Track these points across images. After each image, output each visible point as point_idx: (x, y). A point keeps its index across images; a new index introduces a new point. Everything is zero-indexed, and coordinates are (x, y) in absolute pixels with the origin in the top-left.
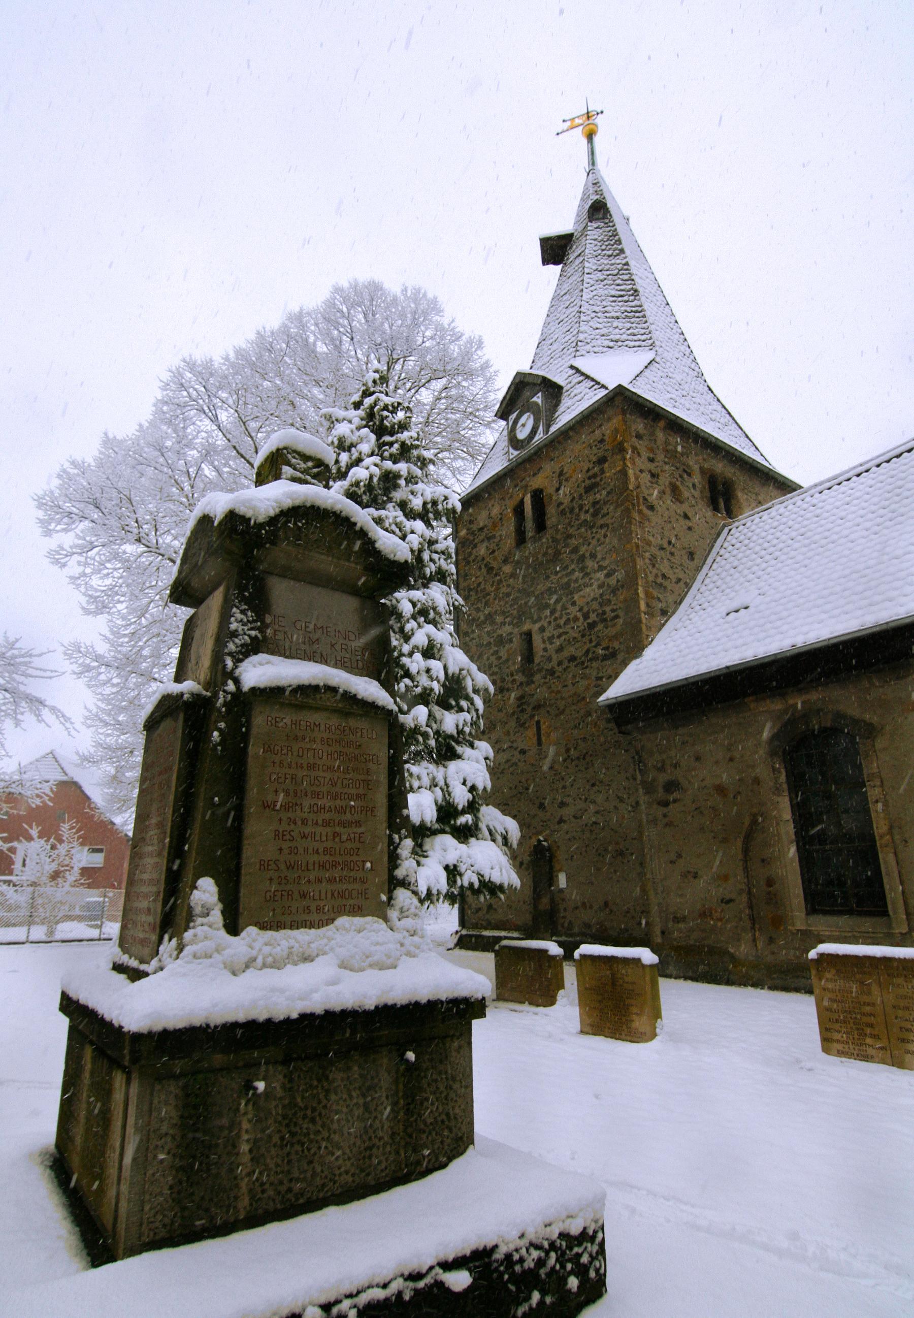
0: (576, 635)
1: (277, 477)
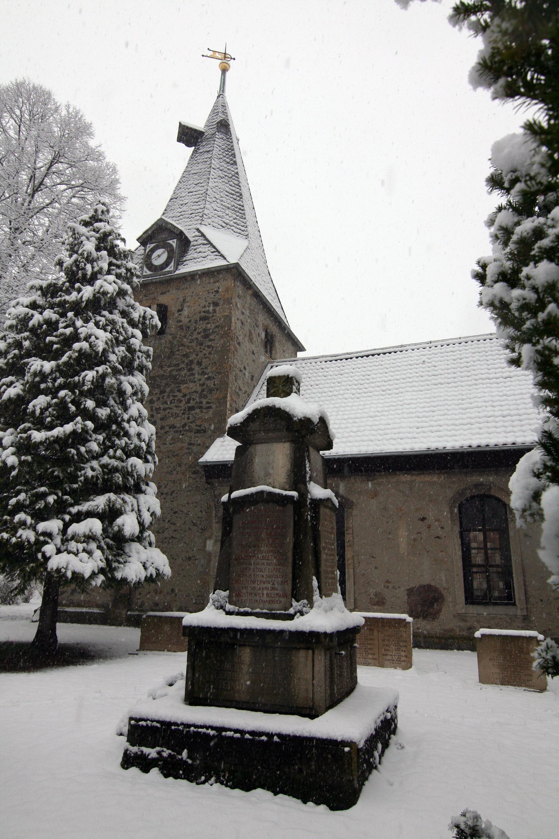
0: (177, 412)
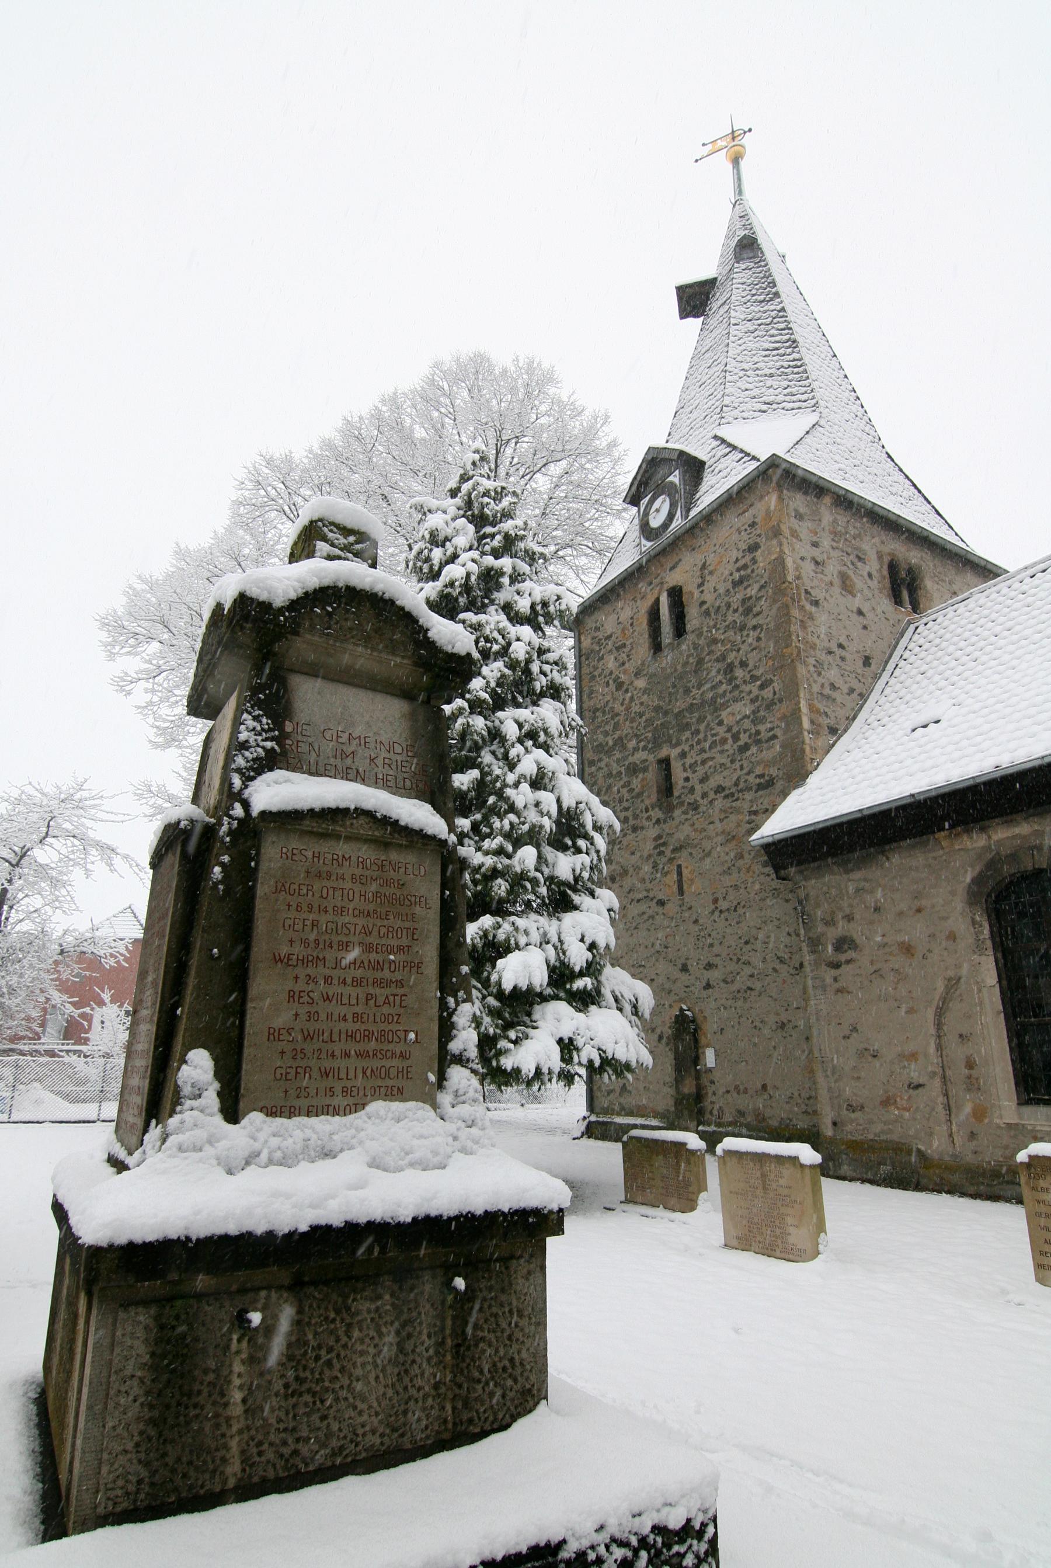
0: (723, 761)
1: (311, 555)
